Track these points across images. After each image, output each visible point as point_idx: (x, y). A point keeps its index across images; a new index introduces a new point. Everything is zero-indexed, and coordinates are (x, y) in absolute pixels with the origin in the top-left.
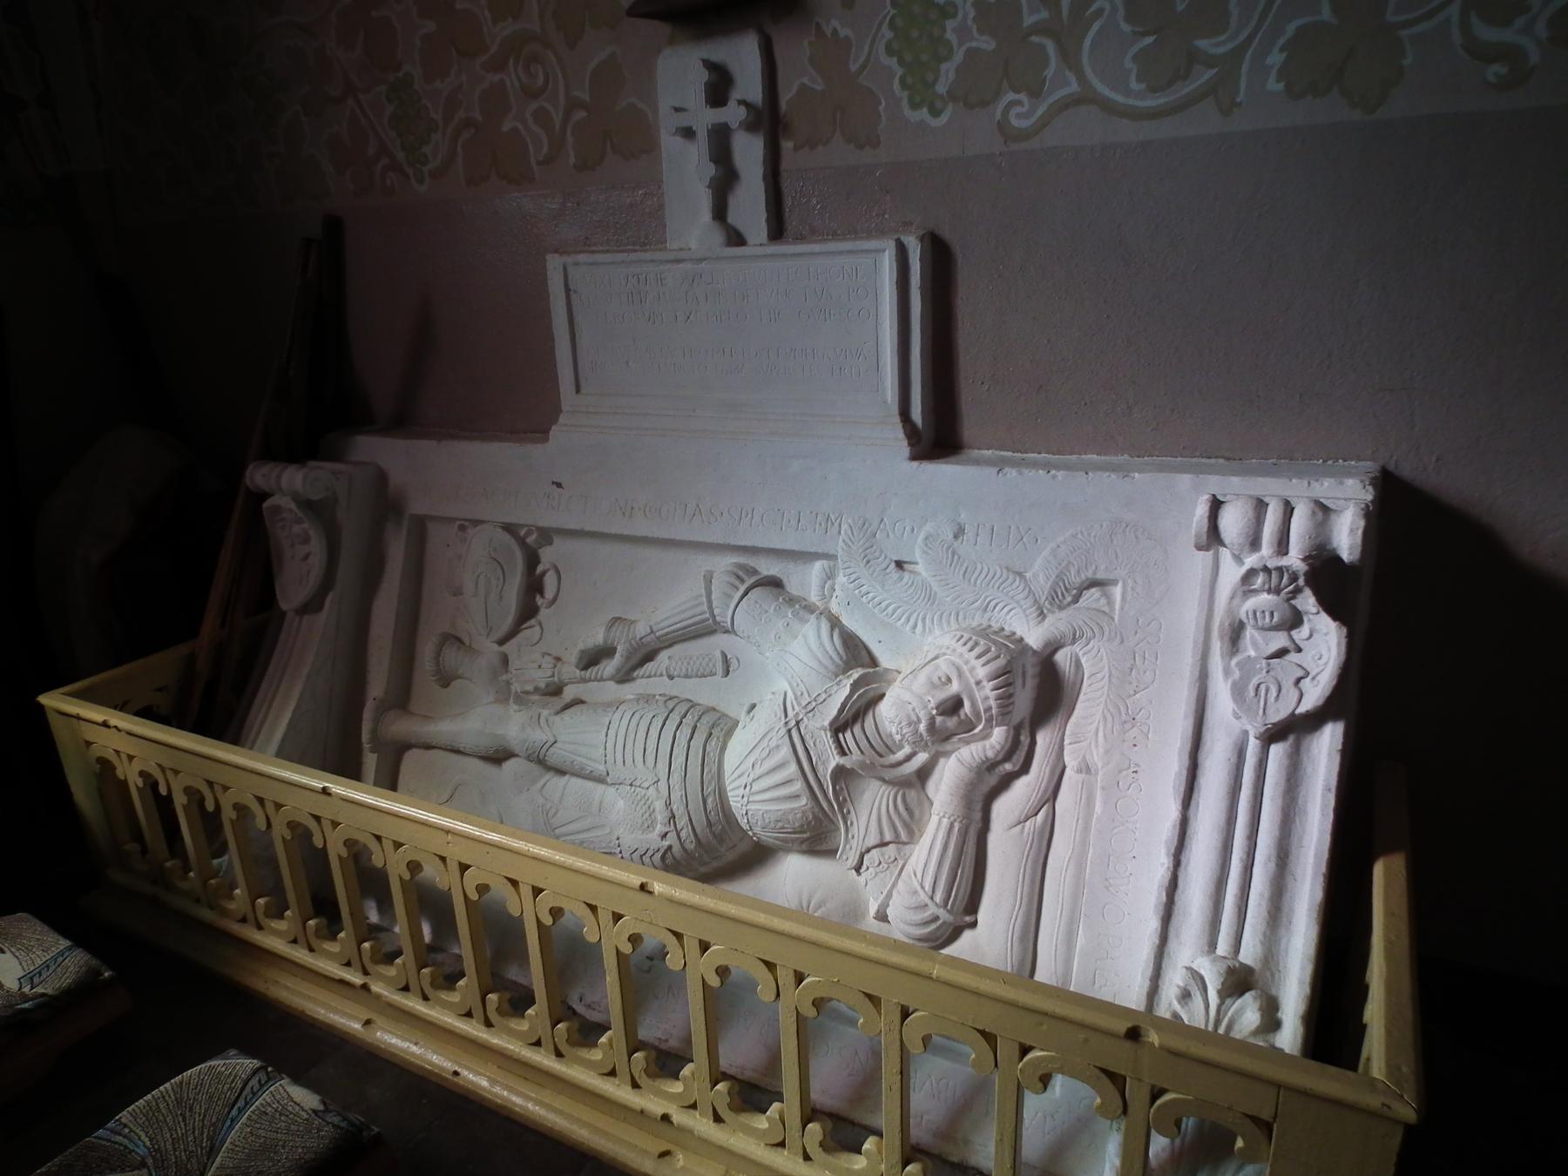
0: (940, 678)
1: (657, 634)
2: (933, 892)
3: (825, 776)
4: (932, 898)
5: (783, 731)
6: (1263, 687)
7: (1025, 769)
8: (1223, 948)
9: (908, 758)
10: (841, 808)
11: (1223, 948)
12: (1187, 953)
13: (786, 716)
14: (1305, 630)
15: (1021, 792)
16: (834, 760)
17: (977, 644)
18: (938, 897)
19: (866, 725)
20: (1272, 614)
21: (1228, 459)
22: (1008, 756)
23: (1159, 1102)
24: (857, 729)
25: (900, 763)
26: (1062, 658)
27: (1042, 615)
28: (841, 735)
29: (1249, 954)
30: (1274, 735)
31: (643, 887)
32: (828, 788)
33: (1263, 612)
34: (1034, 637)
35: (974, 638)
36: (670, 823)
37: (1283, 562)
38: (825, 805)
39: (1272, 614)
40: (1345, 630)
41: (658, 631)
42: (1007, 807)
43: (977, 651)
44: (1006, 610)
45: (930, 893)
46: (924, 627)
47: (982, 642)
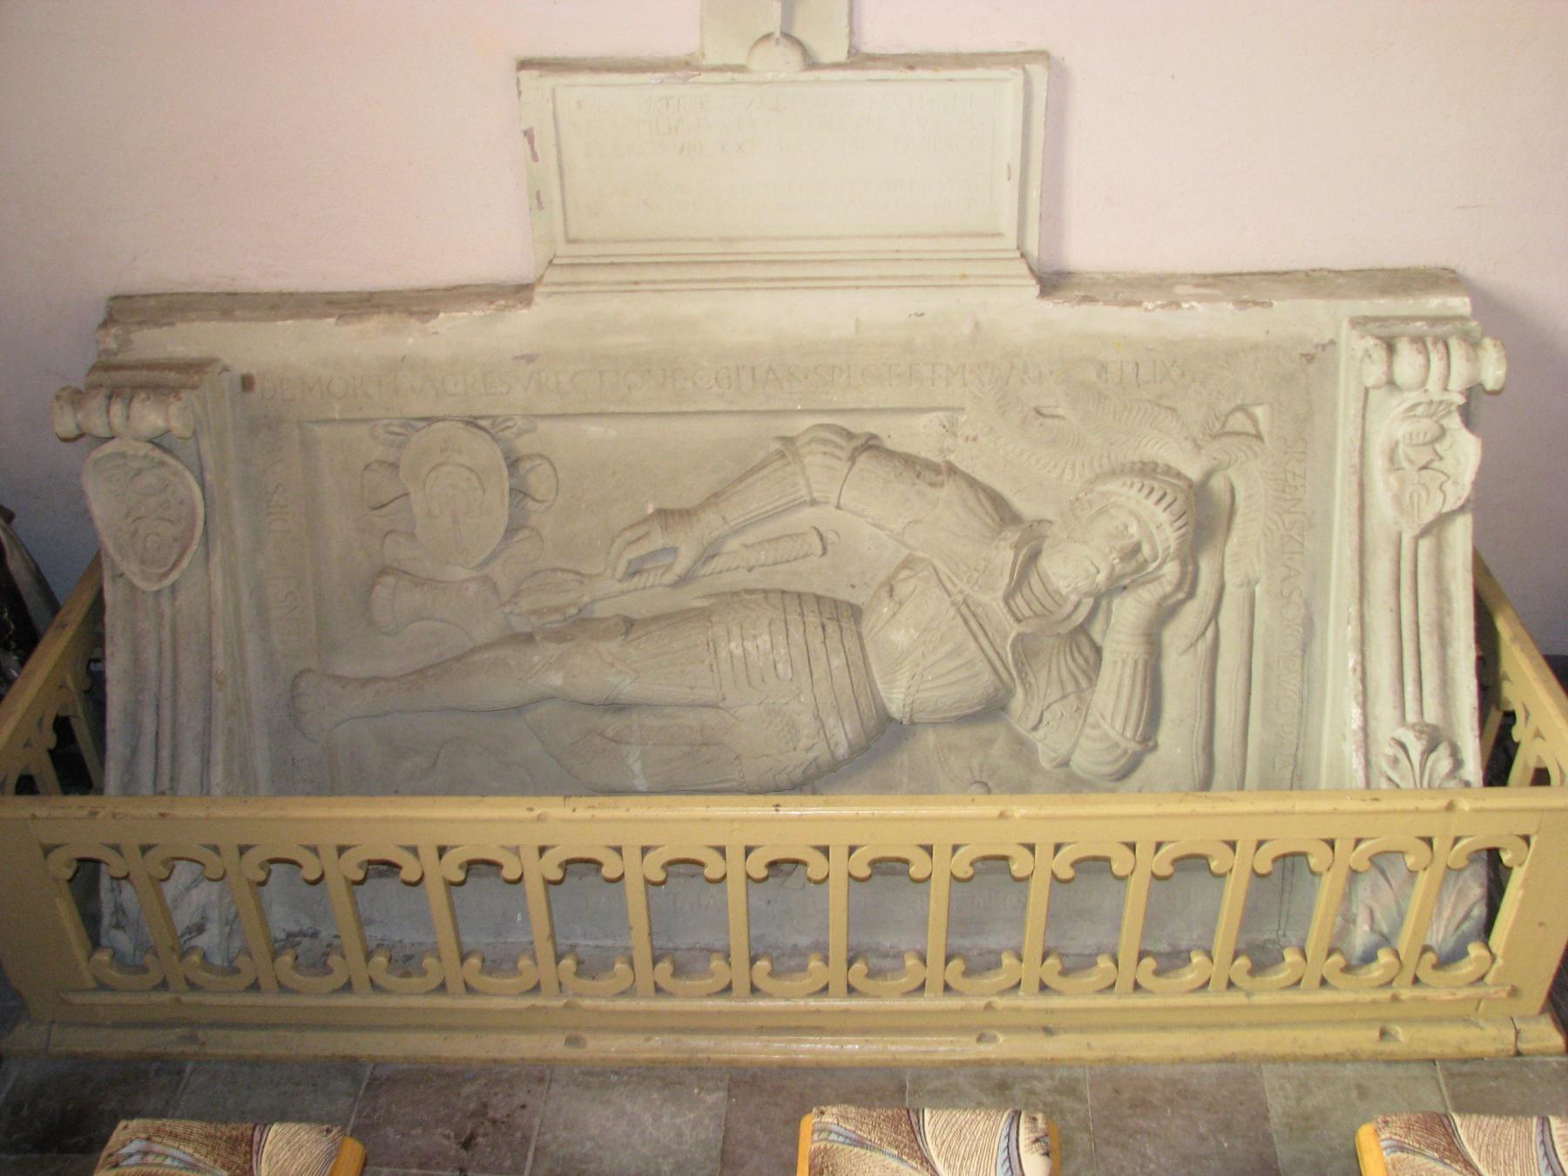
0: (1117, 528)
1: (732, 524)
2: (1124, 729)
3: (1004, 649)
4: (1123, 735)
5: (952, 612)
6: (1415, 495)
7: (1191, 595)
8: (1411, 717)
9: (1076, 607)
10: (1020, 672)
11: (1411, 717)
12: (1386, 728)
13: (949, 595)
14: (1446, 442)
15: (1190, 617)
16: (1014, 630)
17: (1152, 490)
18: (1129, 734)
19: (1032, 582)
20: (1426, 433)
21: (1046, 122)
22: (1179, 587)
23: (1458, 846)
24: (1026, 590)
25: (1069, 616)
26: (1217, 483)
27: (1197, 447)
28: (1011, 602)
29: (1432, 715)
30: (1425, 532)
31: (1002, 816)
32: (1006, 656)
33: (1418, 433)
34: (1193, 472)
35: (1146, 482)
36: (819, 733)
37: (1446, 397)
38: (1004, 675)
39: (1426, 433)
40: (1480, 440)
41: (732, 520)
42: (1175, 636)
43: (1155, 496)
44: (1158, 446)
45: (1121, 731)
46: (1074, 473)
47: (1156, 484)
